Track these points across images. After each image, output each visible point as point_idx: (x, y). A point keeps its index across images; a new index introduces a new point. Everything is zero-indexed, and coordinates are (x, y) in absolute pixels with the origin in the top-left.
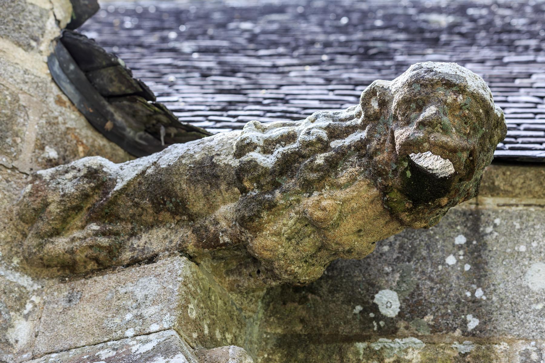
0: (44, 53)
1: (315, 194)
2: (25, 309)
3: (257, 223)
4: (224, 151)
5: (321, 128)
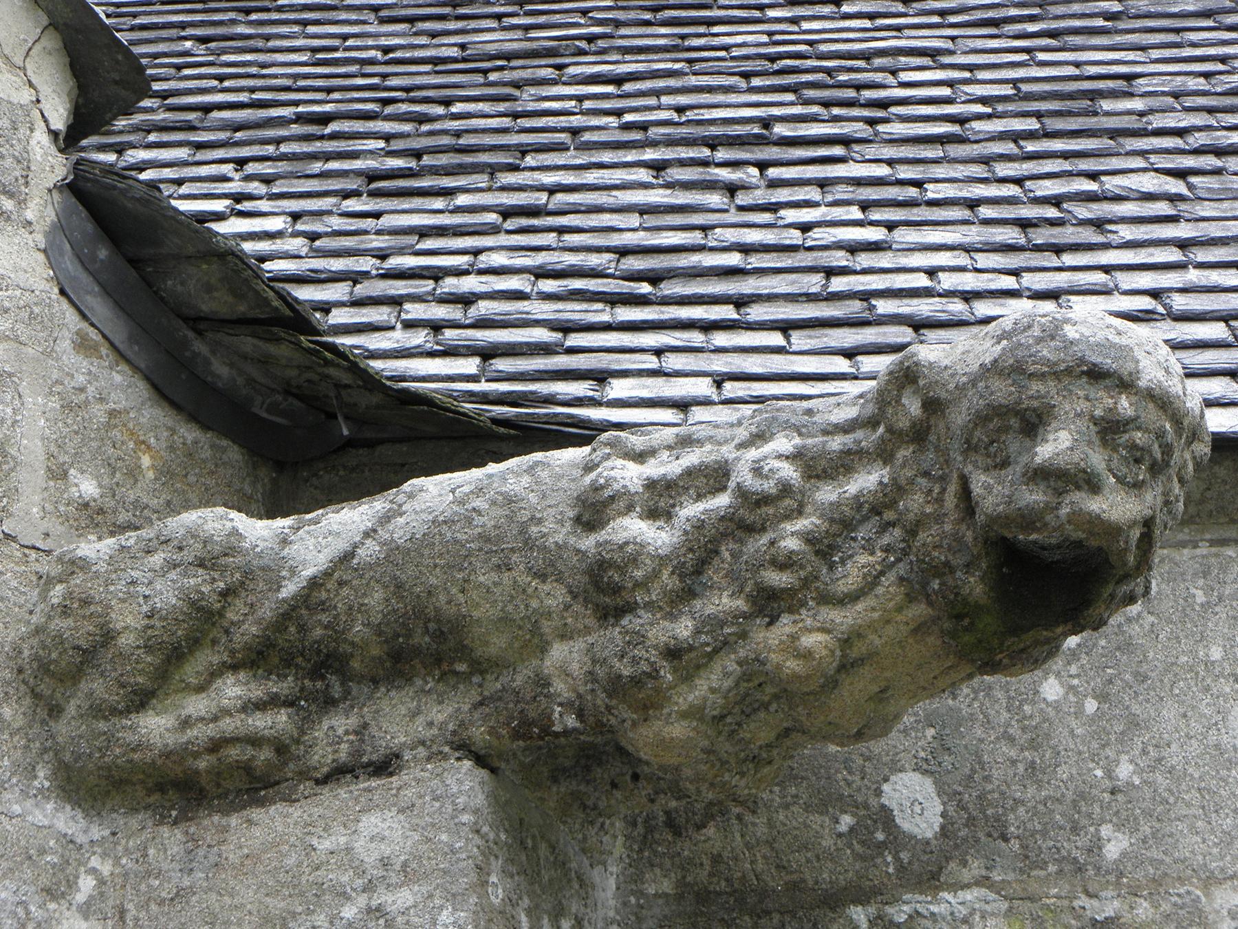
0: (37, 227)
1: (785, 621)
2: (79, 890)
3: (650, 692)
4: (552, 511)
5: (779, 457)
